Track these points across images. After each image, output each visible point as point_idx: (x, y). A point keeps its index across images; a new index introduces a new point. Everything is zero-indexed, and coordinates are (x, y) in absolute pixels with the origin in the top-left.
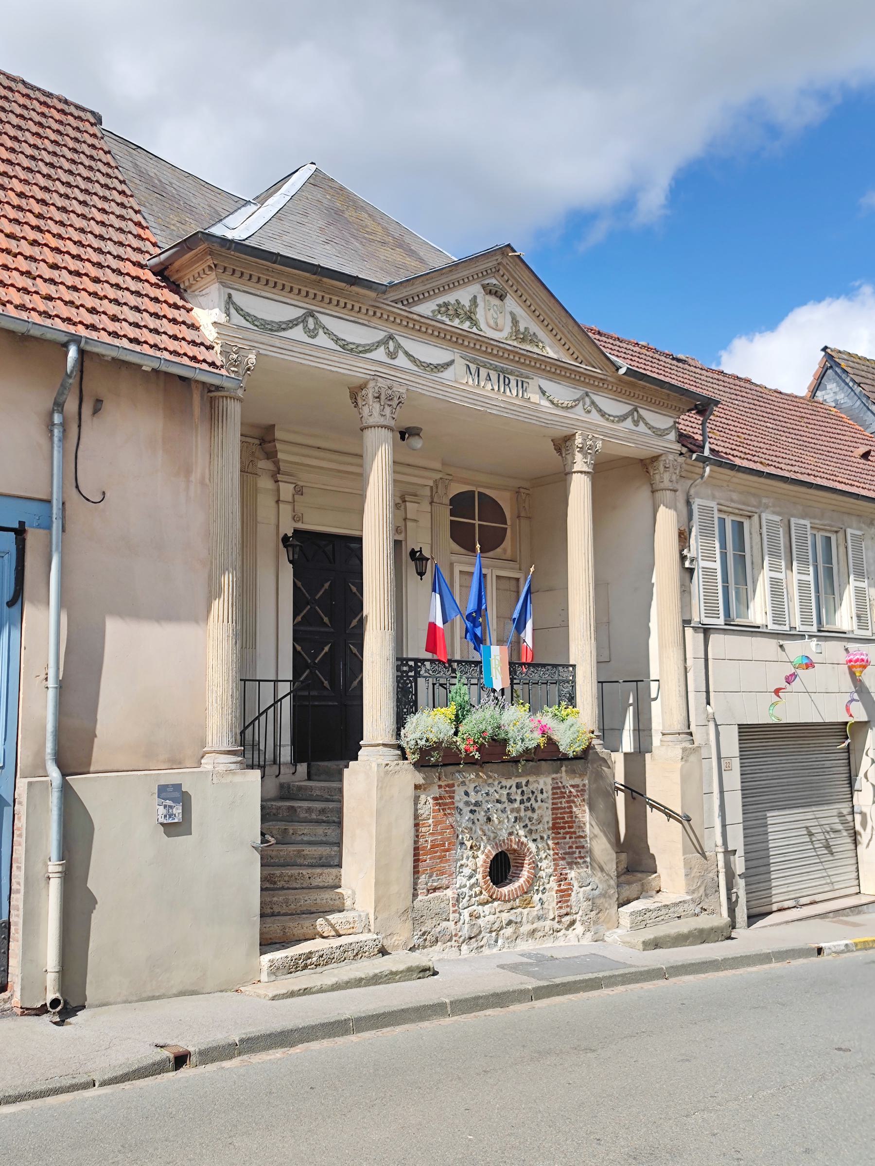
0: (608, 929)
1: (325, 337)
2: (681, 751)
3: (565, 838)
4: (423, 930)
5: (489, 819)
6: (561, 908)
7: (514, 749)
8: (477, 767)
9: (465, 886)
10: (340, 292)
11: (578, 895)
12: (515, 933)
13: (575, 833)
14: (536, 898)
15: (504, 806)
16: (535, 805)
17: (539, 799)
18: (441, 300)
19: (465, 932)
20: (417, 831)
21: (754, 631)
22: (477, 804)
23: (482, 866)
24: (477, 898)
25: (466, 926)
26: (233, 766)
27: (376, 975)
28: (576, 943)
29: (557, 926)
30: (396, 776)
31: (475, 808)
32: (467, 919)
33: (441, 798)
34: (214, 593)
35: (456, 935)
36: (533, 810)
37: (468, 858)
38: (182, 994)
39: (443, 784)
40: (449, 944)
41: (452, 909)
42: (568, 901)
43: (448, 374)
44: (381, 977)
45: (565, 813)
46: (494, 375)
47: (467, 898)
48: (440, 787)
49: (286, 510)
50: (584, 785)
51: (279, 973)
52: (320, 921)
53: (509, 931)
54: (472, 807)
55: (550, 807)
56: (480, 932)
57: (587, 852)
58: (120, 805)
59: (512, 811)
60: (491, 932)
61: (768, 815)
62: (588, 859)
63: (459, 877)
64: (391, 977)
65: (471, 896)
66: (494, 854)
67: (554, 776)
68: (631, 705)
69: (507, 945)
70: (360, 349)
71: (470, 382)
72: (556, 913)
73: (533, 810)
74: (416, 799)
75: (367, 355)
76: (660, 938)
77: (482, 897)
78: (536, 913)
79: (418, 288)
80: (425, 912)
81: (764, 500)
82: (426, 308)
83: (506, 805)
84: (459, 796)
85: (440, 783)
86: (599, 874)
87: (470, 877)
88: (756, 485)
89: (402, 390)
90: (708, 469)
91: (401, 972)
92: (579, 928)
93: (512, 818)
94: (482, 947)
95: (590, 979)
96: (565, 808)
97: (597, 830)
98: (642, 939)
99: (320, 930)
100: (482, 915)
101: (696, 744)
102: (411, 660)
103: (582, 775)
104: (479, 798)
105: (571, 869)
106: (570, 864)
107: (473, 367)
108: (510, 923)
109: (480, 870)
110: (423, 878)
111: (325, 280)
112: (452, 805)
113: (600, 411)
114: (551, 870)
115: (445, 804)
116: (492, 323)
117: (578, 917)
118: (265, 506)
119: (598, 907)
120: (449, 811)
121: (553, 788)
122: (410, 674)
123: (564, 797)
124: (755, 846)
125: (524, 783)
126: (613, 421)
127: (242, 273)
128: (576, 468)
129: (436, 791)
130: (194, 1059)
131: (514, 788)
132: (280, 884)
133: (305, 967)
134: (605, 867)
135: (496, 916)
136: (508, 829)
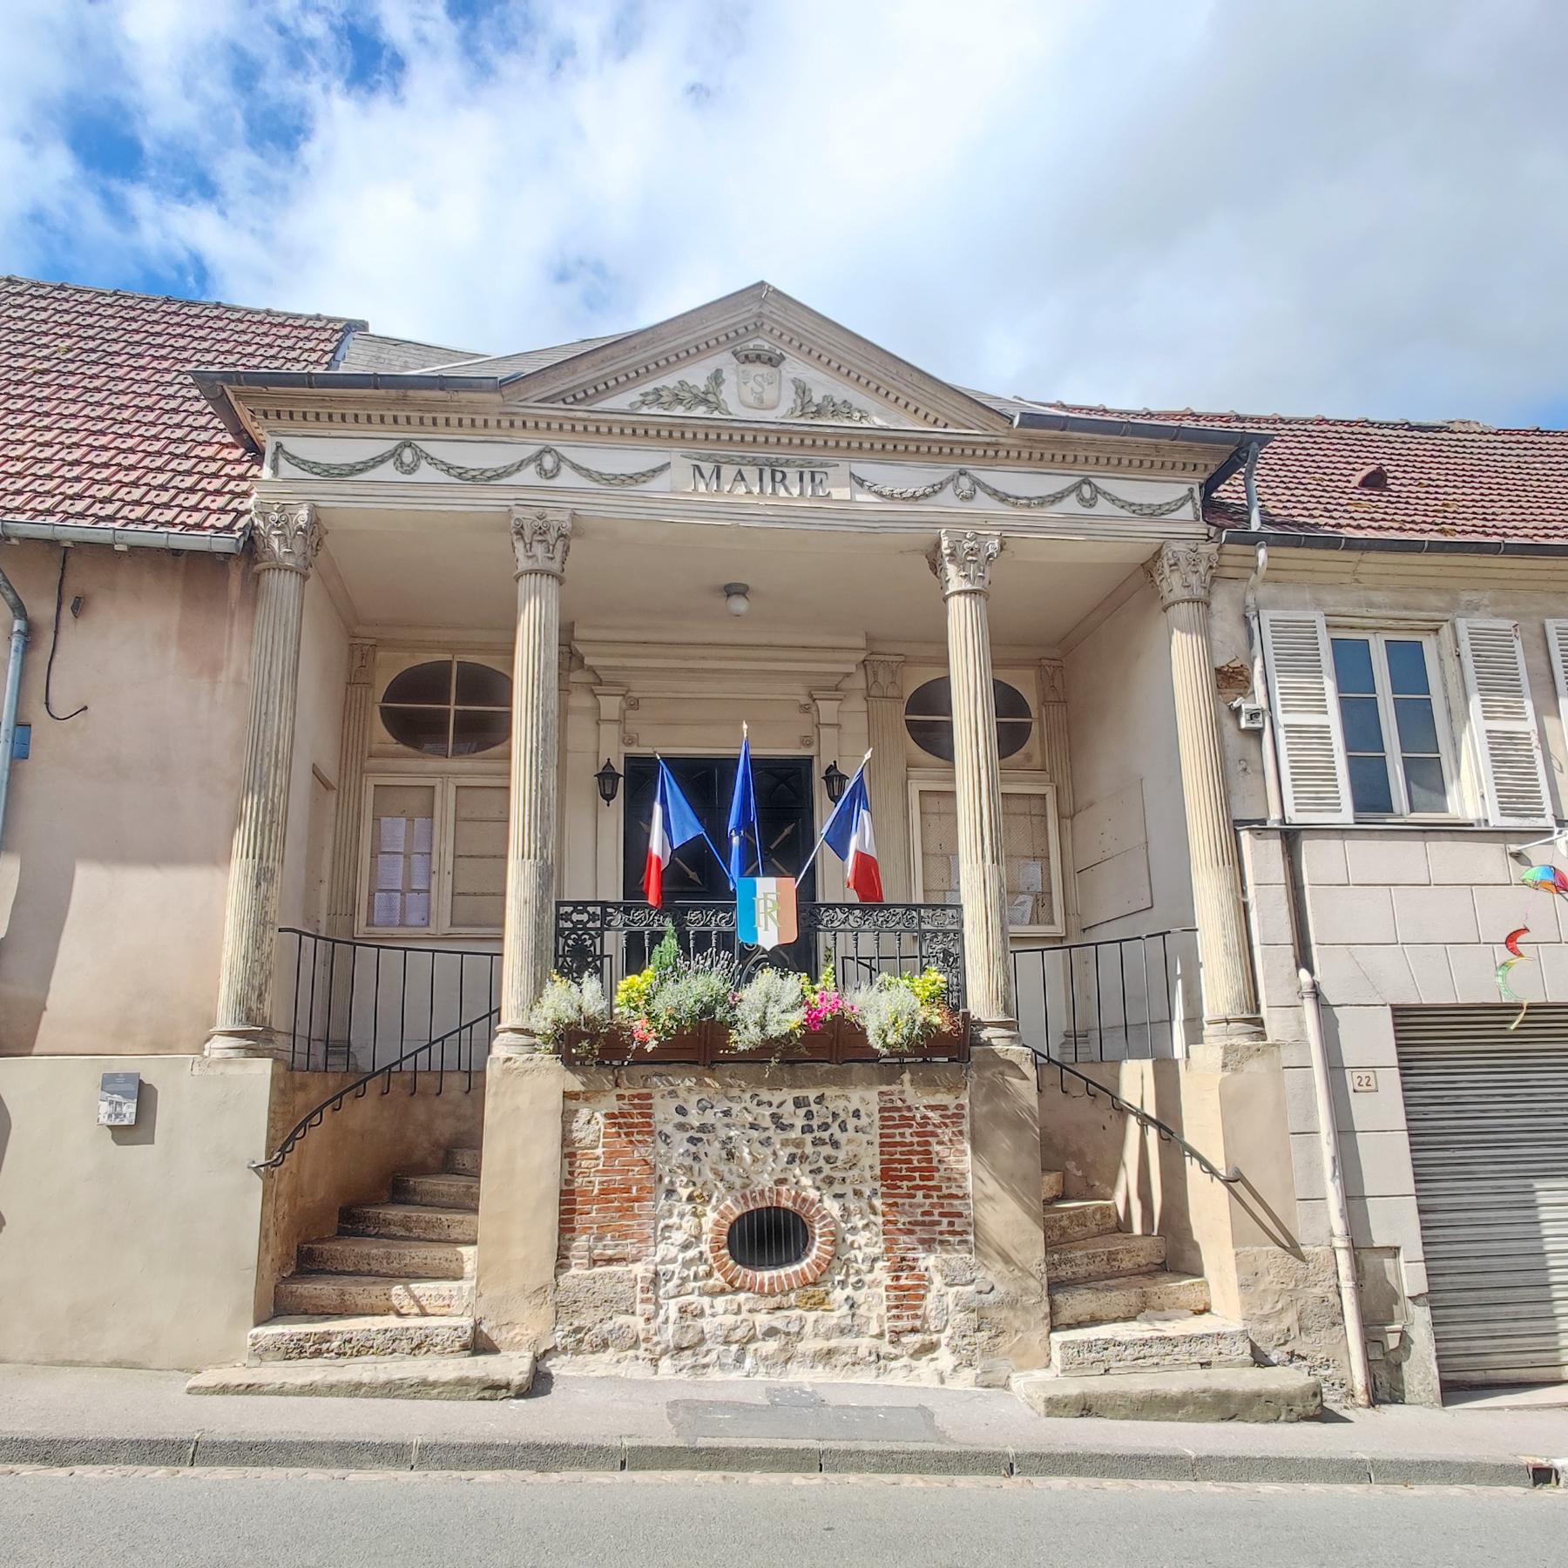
0: (1021, 1368)
1: (432, 468)
2: (1221, 1052)
3: (914, 1196)
4: (576, 1324)
5: (731, 1156)
6: (898, 1317)
7: (745, 1038)
8: (700, 1068)
9: (673, 1260)
10: (444, 405)
12: (783, 1350)
13: (939, 1188)
14: (838, 1295)
15: (766, 1134)
16: (838, 1135)
17: (850, 1127)
18: (649, 387)
19: (669, 1335)
20: (571, 1164)
21: (1461, 831)
22: (703, 1128)
23: (712, 1230)
24: (700, 1284)
25: (671, 1328)
26: (232, 1053)
28: (936, 1384)
29: (886, 1348)
30: (527, 1078)
31: (700, 1135)
32: (674, 1314)
33: (623, 1115)
34: (239, 818)
35: (647, 1340)
36: (836, 1145)
37: (682, 1216)
38: (117, 1364)
39: (627, 1093)
40: (631, 1353)
41: (639, 1296)
42: (918, 1307)
44: (401, 1387)
45: (911, 1153)
46: (751, 473)
48: (620, 1097)
49: (611, 733)
51: (267, 1356)
52: (397, 1289)
53: (771, 1345)
54: (691, 1133)
55: (877, 1140)
56: (702, 1341)
57: (969, 1224)
59: (785, 1143)
60: (727, 1342)
61: (1537, 1186)
62: (971, 1238)
63: (662, 1246)
64: (422, 1389)
65: (684, 1280)
66: (738, 1212)
67: (884, 1088)
68: (1179, 977)
69: (762, 1370)
70: (488, 474)
71: (702, 488)
72: (886, 1326)
73: (836, 1145)
74: (567, 1117)
76: (1098, 1397)
77: (711, 1282)
78: (835, 1321)
79: (585, 374)
80: (581, 1295)
81: (1465, 597)
82: (620, 401)
83: (771, 1133)
84: (664, 1112)
85: (619, 1091)
86: (999, 1266)
87: (686, 1247)
88: (1432, 571)
89: (564, 517)
90: (1262, 554)
91: (444, 1384)
92: (945, 1359)
93: (783, 1155)
94: (705, 1366)
95: (791, 1450)
96: (912, 1144)
97: (992, 1187)
98: (1045, 1396)
99: (396, 1302)
100: (708, 1311)
101: (1269, 1041)
102: (594, 904)
103: (954, 1088)
104: (710, 1117)
105: (929, 1250)
106: (928, 1244)
107: (707, 468)
108: (772, 1332)
109: (708, 1237)
110: (581, 1242)
111: (411, 393)
112: (647, 1128)
113: (994, 493)
114: (877, 1251)
115: (632, 1125)
116: (751, 399)
117: (944, 1338)
118: (581, 728)
119: (992, 1326)
120: (640, 1138)
121: (881, 1110)
122: (590, 925)
123: (911, 1126)
124: (1456, 1247)
125: (812, 1099)
126: (1029, 506)
127: (291, 414)
128: (952, 588)
129: (611, 1103)
131: (790, 1106)
132: (417, 1232)
133: (318, 1353)
134: (1013, 1254)
135: (740, 1318)
136: (776, 1176)
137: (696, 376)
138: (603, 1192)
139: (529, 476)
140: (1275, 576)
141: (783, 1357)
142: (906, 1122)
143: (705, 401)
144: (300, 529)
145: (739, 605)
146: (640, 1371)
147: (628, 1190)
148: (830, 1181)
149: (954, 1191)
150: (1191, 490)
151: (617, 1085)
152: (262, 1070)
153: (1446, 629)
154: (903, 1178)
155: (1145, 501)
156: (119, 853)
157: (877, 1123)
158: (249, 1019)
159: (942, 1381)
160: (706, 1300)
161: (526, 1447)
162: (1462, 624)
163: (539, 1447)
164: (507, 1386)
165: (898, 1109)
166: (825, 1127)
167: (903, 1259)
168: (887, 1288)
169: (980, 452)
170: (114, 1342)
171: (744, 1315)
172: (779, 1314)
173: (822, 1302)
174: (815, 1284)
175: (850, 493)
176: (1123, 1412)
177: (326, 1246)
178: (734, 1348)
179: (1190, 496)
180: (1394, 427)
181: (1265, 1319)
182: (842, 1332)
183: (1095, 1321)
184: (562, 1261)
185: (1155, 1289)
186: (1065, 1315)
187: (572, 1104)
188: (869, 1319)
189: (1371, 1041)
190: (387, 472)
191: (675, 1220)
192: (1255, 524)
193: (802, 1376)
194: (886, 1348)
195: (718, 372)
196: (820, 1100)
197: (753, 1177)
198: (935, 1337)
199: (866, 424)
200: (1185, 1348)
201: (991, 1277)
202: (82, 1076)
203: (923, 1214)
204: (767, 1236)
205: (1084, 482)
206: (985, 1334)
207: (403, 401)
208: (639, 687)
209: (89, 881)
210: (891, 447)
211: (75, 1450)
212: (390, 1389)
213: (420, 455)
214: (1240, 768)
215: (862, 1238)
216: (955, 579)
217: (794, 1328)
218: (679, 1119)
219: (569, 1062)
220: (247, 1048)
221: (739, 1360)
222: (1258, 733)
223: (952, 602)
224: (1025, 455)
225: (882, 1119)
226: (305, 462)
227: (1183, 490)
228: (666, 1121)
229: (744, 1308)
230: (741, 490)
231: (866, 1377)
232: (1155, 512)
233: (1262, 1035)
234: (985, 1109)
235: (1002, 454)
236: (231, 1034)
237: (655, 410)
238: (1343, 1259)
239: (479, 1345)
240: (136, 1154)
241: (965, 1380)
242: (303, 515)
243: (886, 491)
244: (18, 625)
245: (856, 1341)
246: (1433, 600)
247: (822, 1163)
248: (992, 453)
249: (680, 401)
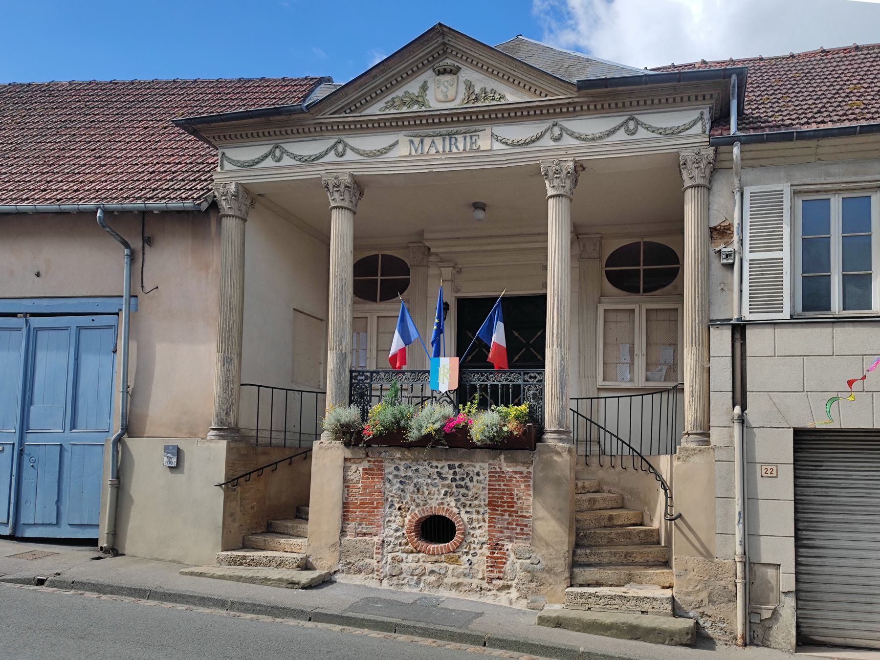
11: (514, 565)
12: (437, 581)
14: (465, 558)
16: (469, 484)
17: (475, 480)
18: (389, 98)
19: (387, 569)
26: (213, 438)
27: (252, 577)
28: (508, 605)
29: (485, 585)
32: (389, 560)
35: (378, 571)
36: (467, 488)
37: (396, 516)
40: (371, 575)
41: (375, 551)
43: (393, 154)
47: (392, 545)
48: (369, 461)
50: (529, 473)
51: (223, 563)
53: (432, 578)
55: (487, 487)
56: (401, 573)
58: (146, 454)
59: (443, 486)
66: (419, 516)
67: (491, 462)
69: (427, 589)
72: (486, 575)
74: (345, 469)
75: (321, 161)
84: (389, 468)
87: (397, 530)
92: (514, 594)
93: (443, 492)
94: (402, 585)
95: (383, 622)
96: (504, 490)
102: (368, 371)
104: (410, 473)
105: (511, 541)
106: (510, 539)
110: (352, 525)
111: (271, 118)
114: (484, 539)
117: (514, 583)
119: (538, 580)
121: (490, 472)
130: (46, 583)
133: (241, 564)
135: (418, 564)
136: (440, 501)
138: (362, 503)
139: (331, 157)
140: (747, 163)
141: (437, 584)
142: (501, 478)
143: (417, 102)
144: (233, 195)
145: (480, 214)
146: (374, 584)
147: (373, 503)
149: (524, 514)
150: (702, 114)
151: (367, 456)
152: (223, 444)
154: (499, 506)
155: (669, 126)
157: (488, 479)
158: (222, 423)
159: (511, 603)
160: (404, 555)
161: (272, 607)
163: (277, 607)
164: (298, 583)
165: (497, 472)
166: (463, 479)
167: (497, 544)
168: (488, 557)
169: (564, 110)
171: (421, 563)
172: (436, 564)
173: (457, 561)
174: (454, 552)
175: (491, 144)
176: (577, 628)
177: (279, 522)
178: (416, 578)
179: (701, 118)
181: (688, 594)
182: (465, 575)
183: (598, 584)
184: (343, 532)
185: (638, 572)
186: (580, 580)
187: (348, 464)
188: (478, 571)
191: (393, 518)
193: (444, 593)
194: (485, 585)
195: (425, 82)
196: (460, 466)
197: (429, 501)
198: (509, 583)
199: (503, 102)
200: (634, 603)
201: (539, 557)
202: (158, 445)
203: (508, 524)
204: (436, 530)
205: (630, 119)
206: (534, 584)
211: (108, 589)
212: (252, 580)
213: (284, 152)
214: (720, 288)
215: (478, 532)
217: (443, 572)
218: (395, 473)
219: (347, 445)
220: (222, 436)
221: (418, 583)
222: (731, 266)
224: (592, 107)
225: (490, 477)
226: (234, 161)
227: (696, 114)
228: (390, 473)
229: (421, 560)
231: (475, 597)
232: (674, 133)
233: (708, 443)
234: (541, 475)
235: (578, 108)
236: (214, 429)
237: (392, 111)
239: (306, 566)
240: (178, 477)
241: (522, 605)
242: (233, 187)
243: (509, 142)
244: (127, 251)
245: (471, 581)
247: (461, 496)
248: (571, 110)
249: (404, 104)
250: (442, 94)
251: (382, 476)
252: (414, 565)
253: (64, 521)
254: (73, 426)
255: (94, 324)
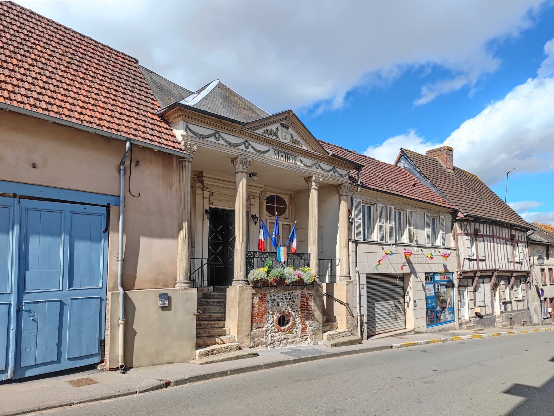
11: (309, 329)
16: (295, 300)
18: (265, 129)
21: (373, 243)
22: (274, 300)
29: (301, 340)
32: (270, 337)
36: (294, 302)
38: (168, 363)
49: (206, 201)
52: (217, 339)
53: (284, 341)
58: (145, 301)
64: (243, 357)
74: (253, 298)
79: (257, 124)
81: (378, 199)
82: (260, 131)
92: (309, 340)
97: (316, 308)
103: (311, 290)
104: (275, 298)
106: (306, 319)
107: (276, 152)
108: (285, 339)
110: (254, 324)
116: (283, 137)
117: (309, 337)
130: (172, 384)
132: (203, 327)
133: (212, 354)
136: (285, 307)
137: (274, 127)
143: (275, 135)
148: (293, 309)
153: (375, 205)
156: (151, 234)
162: (378, 205)
170: (166, 358)
180: (345, 150)
184: (251, 330)
189: (364, 281)
190: (212, 139)
192: (359, 183)
207: (220, 122)
208: (213, 190)
209: (144, 241)
210: (306, 154)
216: (314, 186)
223: (312, 190)
230: (282, 159)
231: (298, 345)
238: (359, 317)
240: (167, 313)
246: (375, 199)
250: (285, 136)
251: (266, 301)
252: (278, 337)
253: (66, 355)
254: (71, 285)
255: (85, 211)
